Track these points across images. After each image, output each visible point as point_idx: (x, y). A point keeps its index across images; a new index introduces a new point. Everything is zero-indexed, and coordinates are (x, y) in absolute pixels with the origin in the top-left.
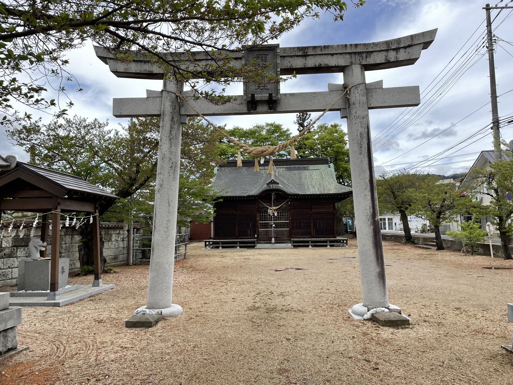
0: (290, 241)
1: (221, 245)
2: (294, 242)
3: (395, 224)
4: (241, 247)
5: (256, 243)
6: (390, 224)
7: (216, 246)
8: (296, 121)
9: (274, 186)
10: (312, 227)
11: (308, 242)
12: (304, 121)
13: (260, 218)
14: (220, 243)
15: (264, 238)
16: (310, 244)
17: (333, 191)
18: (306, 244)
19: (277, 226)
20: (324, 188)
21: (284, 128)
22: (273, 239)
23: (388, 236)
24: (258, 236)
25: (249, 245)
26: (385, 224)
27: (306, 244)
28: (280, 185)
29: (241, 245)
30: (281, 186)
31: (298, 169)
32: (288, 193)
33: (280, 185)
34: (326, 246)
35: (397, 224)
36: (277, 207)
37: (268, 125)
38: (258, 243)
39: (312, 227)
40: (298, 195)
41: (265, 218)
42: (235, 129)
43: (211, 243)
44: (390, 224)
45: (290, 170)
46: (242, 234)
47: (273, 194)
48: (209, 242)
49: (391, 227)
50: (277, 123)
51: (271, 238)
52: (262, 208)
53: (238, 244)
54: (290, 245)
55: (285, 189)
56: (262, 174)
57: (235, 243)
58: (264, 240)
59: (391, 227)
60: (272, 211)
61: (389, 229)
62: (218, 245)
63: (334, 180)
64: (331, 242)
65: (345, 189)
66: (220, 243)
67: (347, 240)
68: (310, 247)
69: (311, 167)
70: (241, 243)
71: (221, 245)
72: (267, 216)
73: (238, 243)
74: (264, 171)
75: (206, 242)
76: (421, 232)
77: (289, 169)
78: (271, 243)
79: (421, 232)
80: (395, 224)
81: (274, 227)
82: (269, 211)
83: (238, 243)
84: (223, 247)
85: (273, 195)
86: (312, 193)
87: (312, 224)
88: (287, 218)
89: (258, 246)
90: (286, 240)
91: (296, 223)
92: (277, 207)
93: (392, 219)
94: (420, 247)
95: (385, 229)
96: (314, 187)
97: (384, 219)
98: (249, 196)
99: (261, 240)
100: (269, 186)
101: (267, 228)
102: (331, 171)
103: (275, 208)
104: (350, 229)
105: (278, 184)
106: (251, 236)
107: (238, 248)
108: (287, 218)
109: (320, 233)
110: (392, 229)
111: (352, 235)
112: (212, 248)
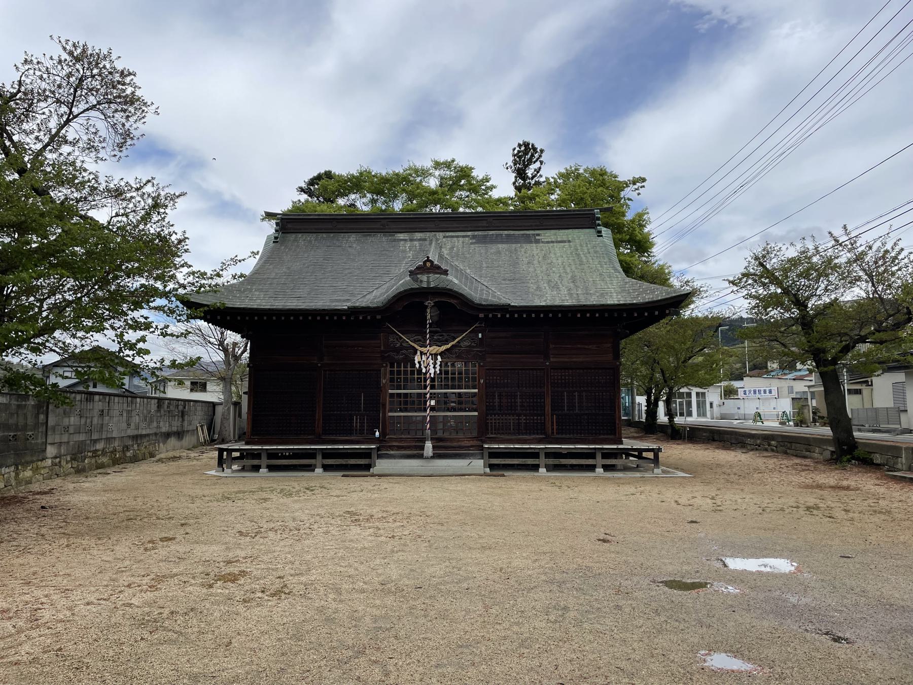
0: (480, 452)
1: (264, 461)
2: (494, 454)
3: (711, 404)
4: (326, 468)
5: (374, 455)
6: (701, 405)
7: (250, 462)
8: (510, 163)
9: (429, 280)
10: (548, 409)
11: (535, 455)
12: (526, 166)
13: (392, 380)
14: (264, 456)
15: (401, 440)
16: (542, 460)
17: (614, 298)
18: (530, 461)
19: (443, 403)
20: (587, 288)
21: (478, 174)
22: (429, 445)
23: (753, 436)
24: (383, 434)
25: (352, 461)
26: (689, 404)
27: (530, 461)
28: (450, 277)
29: (551, 461)
30: (454, 281)
31: (509, 240)
32: (477, 301)
33: (450, 277)
34: (592, 468)
35: (714, 405)
36: (444, 348)
37: (437, 165)
38: (380, 457)
39: (548, 409)
40: (505, 309)
41: (406, 380)
42: (361, 174)
43: (237, 454)
44: (701, 405)
45: (485, 243)
46: (337, 427)
47: (429, 303)
48: (230, 451)
49: (702, 413)
50: (462, 162)
51: (423, 441)
52: (397, 351)
53: (319, 460)
54: (478, 464)
55: (466, 290)
56: (404, 251)
57: (311, 455)
58: (399, 448)
59: (702, 413)
60: (428, 361)
61: (699, 415)
62: (256, 462)
63: (616, 270)
64: (607, 455)
65: (653, 292)
66: (264, 456)
67: (656, 452)
68: (542, 470)
69: (548, 235)
70: (326, 454)
71: (264, 461)
72: (412, 373)
73: (319, 457)
74: (408, 244)
75: (221, 451)
76: (796, 425)
77: (483, 240)
78: (421, 456)
79: (796, 425)
80: (711, 404)
81: (433, 409)
82: (417, 359)
83: (319, 457)
84: (271, 468)
85: (428, 308)
86: (549, 303)
87: (548, 401)
88: (474, 379)
89: (382, 465)
90: (468, 448)
91: (500, 396)
92: (444, 348)
93: (703, 394)
94: (902, 479)
95: (690, 414)
96: (556, 287)
97: (689, 395)
98: (354, 311)
99: (391, 448)
100: (416, 280)
101: (406, 410)
102: (605, 246)
103: (435, 349)
104: (626, 415)
105: (445, 272)
106: (361, 432)
107: (319, 470)
108: (474, 379)
109: (569, 429)
110: (704, 415)
111: (632, 430)
112: (243, 469)
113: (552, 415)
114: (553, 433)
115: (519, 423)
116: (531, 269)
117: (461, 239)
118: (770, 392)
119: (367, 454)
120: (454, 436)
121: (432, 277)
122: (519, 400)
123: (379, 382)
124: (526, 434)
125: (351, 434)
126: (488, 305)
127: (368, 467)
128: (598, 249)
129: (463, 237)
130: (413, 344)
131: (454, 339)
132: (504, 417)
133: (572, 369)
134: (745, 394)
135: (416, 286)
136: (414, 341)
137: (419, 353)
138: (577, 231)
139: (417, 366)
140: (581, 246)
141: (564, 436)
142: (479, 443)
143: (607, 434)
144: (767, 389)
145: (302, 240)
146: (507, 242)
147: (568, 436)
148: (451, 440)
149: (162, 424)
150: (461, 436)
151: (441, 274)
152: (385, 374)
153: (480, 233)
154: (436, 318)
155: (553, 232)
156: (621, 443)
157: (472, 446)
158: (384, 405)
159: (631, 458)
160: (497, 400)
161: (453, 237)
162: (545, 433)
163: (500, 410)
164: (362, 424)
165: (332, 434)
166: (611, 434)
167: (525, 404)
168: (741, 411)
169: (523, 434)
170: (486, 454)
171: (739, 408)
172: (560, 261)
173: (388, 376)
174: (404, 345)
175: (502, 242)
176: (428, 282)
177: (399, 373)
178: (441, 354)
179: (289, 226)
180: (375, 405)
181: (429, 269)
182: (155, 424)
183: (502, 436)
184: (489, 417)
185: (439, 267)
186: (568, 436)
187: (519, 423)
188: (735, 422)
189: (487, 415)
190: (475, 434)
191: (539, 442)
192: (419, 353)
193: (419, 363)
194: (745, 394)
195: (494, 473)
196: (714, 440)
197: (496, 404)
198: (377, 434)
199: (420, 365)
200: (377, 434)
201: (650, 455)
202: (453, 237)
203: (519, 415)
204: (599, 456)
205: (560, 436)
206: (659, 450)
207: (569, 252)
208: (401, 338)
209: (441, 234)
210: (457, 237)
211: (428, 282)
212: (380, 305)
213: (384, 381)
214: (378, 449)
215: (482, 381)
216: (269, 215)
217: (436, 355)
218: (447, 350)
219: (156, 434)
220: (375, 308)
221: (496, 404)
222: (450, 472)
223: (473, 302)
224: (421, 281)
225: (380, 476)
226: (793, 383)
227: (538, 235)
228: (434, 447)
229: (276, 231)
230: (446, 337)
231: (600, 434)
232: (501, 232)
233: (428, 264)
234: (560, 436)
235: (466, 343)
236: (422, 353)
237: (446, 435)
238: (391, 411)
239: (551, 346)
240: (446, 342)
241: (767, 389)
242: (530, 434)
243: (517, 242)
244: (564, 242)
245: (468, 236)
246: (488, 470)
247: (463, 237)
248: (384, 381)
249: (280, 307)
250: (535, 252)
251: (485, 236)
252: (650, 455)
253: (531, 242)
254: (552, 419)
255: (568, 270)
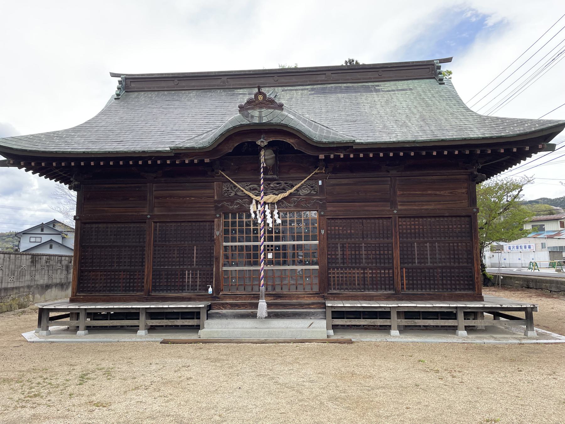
2: (338, 314)
5: (203, 315)
10: (397, 261)
11: (385, 314)
13: (226, 232)
22: (263, 304)
24: (217, 290)
27: (379, 322)
29: (405, 322)
36: (281, 196)
38: (209, 316)
39: (397, 261)
45: (324, 93)
46: (168, 282)
52: (232, 200)
57: (134, 315)
58: (233, 306)
60: (264, 210)
68: (395, 332)
70: (153, 315)
73: (143, 317)
78: (254, 316)
82: (252, 208)
87: (397, 254)
89: (212, 328)
90: (308, 305)
91: (343, 247)
92: (281, 196)
96: (404, 125)
98: (178, 154)
99: (224, 306)
100: (247, 116)
103: (271, 198)
105: (281, 107)
109: (422, 281)
113: (401, 268)
114: (403, 288)
115: (364, 277)
116: (375, 112)
117: (300, 92)
118: (530, 247)
119: (195, 314)
120: (293, 292)
121: (265, 111)
122: (364, 252)
123: (212, 234)
124: (373, 289)
125: (183, 290)
126: (329, 143)
127: (197, 328)
128: (442, 94)
129: (302, 90)
130: (247, 192)
131: (292, 186)
132: (348, 271)
133: (422, 217)
134: (510, 249)
135: (246, 122)
136: (250, 190)
137: (254, 202)
138: (416, 81)
139: (253, 215)
140: (424, 92)
141: (415, 292)
142: (321, 300)
143: (464, 289)
144: (527, 245)
145: (143, 97)
146: (347, 92)
147: (420, 292)
148: (290, 297)
149: (37, 277)
150: (300, 291)
151: (274, 108)
152: (219, 226)
153: (319, 86)
154: (271, 162)
155: (392, 83)
156: (481, 299)
157: (313, 304)
158: (218, 259)
159: (502, 319)
160: (339, 252)
161: (292, 90)
162: (394, 289)
163: (343, 263)
164: (194, 278)
165: (163, 290)
166: (469, 289)
167: (371, 257)
168: (507, 262)
169: (369, 290)
170: (329, 314)
171: (505, 259)
172: (404, 104)
173: (222, 228)
174: (239, 194)
175: (340, 92)
176: (260, 117)
177: (234, 223)
178: (279, 202)
179: (133, 85)
180: (209, 258)
181: (261, 103)
182: (28, 277)
183: (346, 292)
184: (331, 271)
185: (272, 102)
186: (420, 292)
187: (364, 277)
188: (515, 270)
189: (329, 269)
190: (316, 289)
191: (388, 298)
192: (254, 202)
193: (255, 212)
194: (510, 249)
195: (339, 337)
196: (528, 287)
197: (339, 256)
198: (210, 290)
199: (256, 215)
200: (210, 290)
201: (522, 314)
202: (292, 90)
203: (364, 269)
204: (461, 316)
205: (411, 292)
206: (534, 308)
207: (412, 97)
208: (235, 187)
209: (280, 88)
210: (296, 90)
211: (260, 117)
212: (207, 145)
213: (218, 233)
214: (210, 307)
215: (323, 232)
216: (114, 75)
217: (272, 204)
218: (284, 198)
219: (29, 287)
220: (200, 148)
221: (339, 256)
222: (288, 338)
223: (311, 140)
224: (252, 117)
225: (205, 342)
226: (544, 241)
227: (378, 86)
228: (269, 305)
229: (119, 88)
230: (283, 185)
231: (456, 289)
232: (340, 85)
233: (260, 97)
234: (411, 292)
235: (306, 192)
236: (257, 202)
237: (285, 291)
238: (224, 265)
239: (398, 193)
240: (284, 190)
241: (527, 245)
242: (377, 289)
243: (356, 92)
244: (406, 90)
245: (307, 89)
246: (331, 332)
247: (302, 90)
248: (218, 233)
249: (96, 150)
250: (376, 99)
251: (323, 89)
252: (522, 314)
253: (371, 91)
254: (402, 272)
255: (415, 111)
